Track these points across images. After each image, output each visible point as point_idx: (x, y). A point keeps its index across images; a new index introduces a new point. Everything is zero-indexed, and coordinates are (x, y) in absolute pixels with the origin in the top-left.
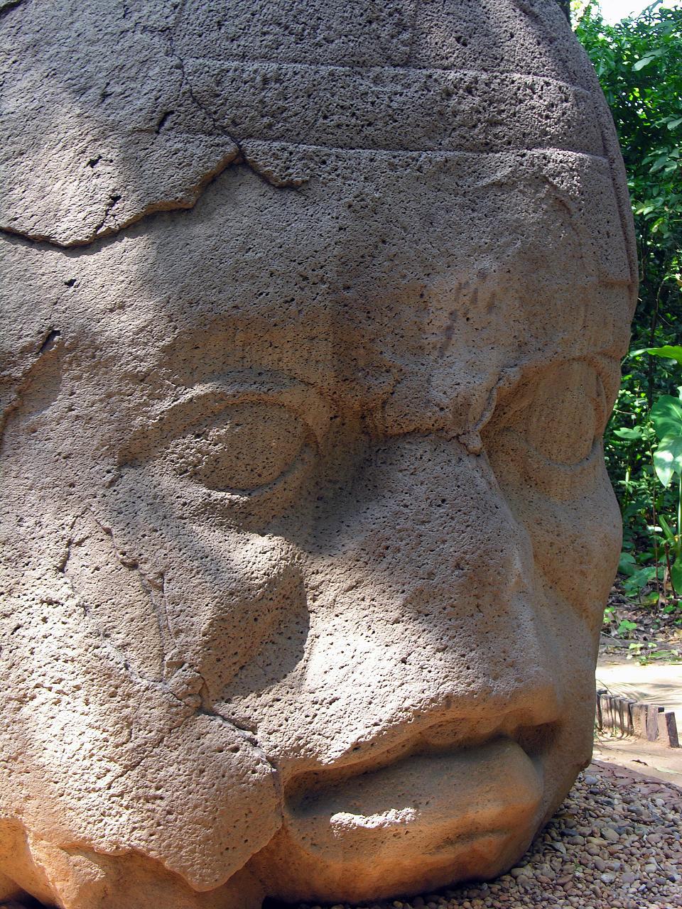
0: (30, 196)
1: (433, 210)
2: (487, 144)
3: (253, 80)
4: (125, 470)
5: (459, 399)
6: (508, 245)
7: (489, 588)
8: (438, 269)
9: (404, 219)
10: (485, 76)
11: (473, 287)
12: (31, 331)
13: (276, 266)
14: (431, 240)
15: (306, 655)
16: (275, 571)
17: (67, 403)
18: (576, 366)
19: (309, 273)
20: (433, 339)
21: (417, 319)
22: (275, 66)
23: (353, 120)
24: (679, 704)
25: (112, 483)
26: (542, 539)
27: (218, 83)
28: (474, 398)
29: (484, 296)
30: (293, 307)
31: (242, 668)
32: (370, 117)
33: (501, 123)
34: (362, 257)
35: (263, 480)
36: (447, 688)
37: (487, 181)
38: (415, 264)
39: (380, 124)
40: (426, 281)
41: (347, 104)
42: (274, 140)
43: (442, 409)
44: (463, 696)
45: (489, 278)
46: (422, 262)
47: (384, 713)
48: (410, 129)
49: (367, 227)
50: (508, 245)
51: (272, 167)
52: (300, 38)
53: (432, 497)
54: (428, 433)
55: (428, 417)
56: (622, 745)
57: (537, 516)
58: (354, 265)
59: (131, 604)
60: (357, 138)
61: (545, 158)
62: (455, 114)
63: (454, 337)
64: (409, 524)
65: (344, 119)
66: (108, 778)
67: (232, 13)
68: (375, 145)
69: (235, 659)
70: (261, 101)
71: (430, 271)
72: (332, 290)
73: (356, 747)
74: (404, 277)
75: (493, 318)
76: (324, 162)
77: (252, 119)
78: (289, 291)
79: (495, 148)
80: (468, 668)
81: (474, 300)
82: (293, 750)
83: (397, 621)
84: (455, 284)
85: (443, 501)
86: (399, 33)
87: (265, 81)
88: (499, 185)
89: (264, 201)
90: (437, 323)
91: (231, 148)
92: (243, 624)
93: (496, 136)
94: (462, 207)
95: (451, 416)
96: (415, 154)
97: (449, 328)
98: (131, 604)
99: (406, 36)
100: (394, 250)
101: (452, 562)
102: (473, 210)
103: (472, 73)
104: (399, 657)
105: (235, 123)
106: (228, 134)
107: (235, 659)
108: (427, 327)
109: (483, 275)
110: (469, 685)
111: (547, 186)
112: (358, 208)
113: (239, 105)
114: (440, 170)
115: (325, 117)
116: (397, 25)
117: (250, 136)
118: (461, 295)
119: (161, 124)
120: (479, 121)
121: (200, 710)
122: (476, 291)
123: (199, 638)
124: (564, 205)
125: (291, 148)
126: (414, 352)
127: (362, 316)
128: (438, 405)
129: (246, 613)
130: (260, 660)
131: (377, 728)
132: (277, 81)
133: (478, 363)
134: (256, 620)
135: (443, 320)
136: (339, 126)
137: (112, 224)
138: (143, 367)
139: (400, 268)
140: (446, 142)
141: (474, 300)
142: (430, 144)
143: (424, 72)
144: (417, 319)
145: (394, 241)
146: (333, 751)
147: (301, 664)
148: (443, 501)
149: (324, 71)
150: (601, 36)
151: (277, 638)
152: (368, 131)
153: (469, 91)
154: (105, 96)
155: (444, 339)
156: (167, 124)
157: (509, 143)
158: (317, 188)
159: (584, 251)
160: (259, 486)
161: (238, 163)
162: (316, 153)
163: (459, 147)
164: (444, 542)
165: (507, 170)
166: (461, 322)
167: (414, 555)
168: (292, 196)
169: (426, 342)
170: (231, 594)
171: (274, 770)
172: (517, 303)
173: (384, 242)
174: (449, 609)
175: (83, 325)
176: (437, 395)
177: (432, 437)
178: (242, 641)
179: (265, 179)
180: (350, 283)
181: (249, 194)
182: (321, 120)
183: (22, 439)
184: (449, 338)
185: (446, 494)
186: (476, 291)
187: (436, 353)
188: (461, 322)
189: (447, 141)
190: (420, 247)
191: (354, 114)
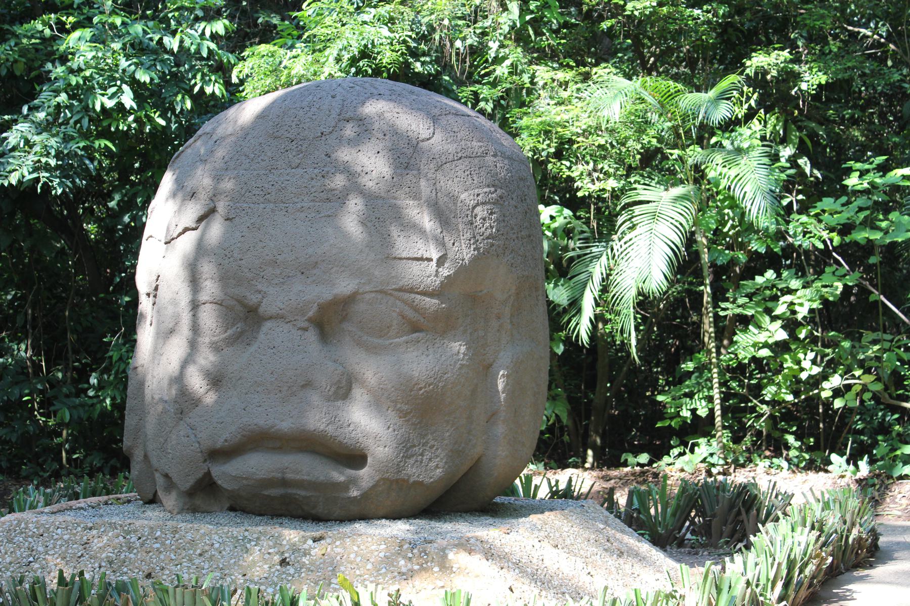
19: (227, 253)
32: (269, 191)
39: (273, 193)
65: (257, 193)
163: (313, 201)
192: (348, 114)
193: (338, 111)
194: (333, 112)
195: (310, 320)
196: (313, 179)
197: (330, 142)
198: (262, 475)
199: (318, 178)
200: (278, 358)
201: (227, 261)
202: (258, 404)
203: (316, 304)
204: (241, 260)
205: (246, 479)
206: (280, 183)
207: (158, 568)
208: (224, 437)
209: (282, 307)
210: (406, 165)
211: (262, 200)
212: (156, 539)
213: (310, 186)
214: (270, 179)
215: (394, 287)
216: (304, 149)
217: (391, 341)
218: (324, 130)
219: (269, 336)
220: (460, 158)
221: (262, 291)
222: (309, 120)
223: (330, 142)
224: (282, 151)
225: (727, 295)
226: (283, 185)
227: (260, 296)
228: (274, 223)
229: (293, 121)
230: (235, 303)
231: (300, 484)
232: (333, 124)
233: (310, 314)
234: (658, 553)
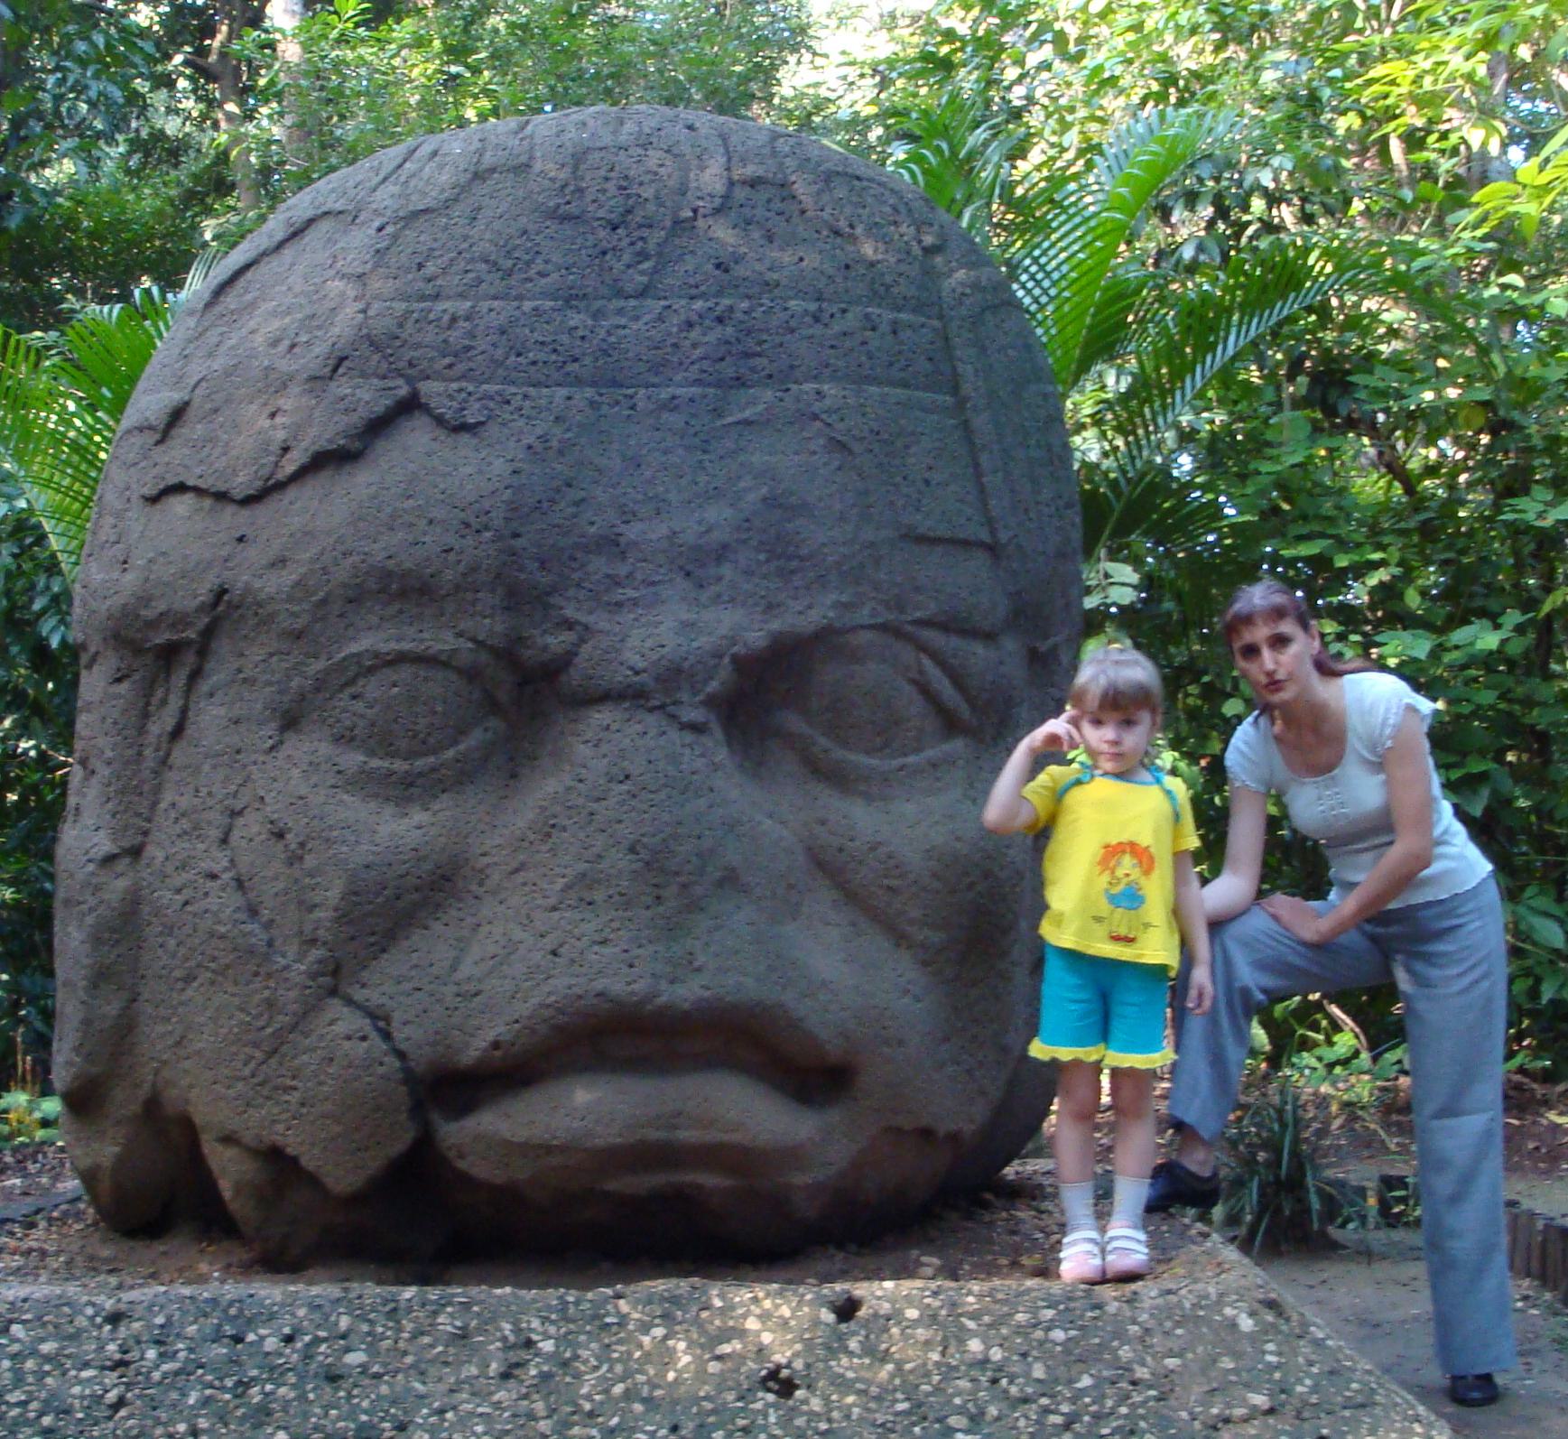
0: (216, 452)
1: (644, 452)
3: (439, 319)
4: (286, 735)
10: (745, 305)
12: (203, 592)
13: (438, 513)
17: (236, 665)
19: (472, 520)
22: (469, 304)
23: (554, 357)
25: (272, 748)
27: (401, 325)
30: (452, 557)
32: (577, 352)
33: (759, 355)
37: (730, 420)
39: (588, 360)
41: (548, 339)
42: (452, 380)
47: (523, 1009)
51: (446, 408)
52: (509, 273)
55: (621, 677)
56: (1460, 975)
59: (276, 878)
62: (694, 346)
64: (581, 801)
65: (541, 356)
66: (252, 1065)
67: (437, 253)
68: (579, 382)
70: (445, 341)
72: (499, 537)
73: (496, 1045)
74: (592, 523)
76: (508, 402)
77: (432, 359)
78: (451, 540)
83: (554, 909)
85: (627, 777)
86: (639, 262)
87: (454, 319)
88: (747, 423)
89: (435, 446)
91: (403, 391)
93: (753, 370)
96: (630, 391)
98: (276, 878)
99: (646, 265)
101: (626, 844)
102: (705, 452)
103: (727, 302)
104: (549, 947)
106: (402, 376)
110: (629, 984)
113: (418, 346)
115: (519, 355)
116: (639, 254)
117: (428, 378)
119: (335, 370)
121: (333, 992)
123: (330, 914)
125: (471, 388)
128: (631, 668)
131: (516, 1026)
132: (467, 319)
137: (281, 475)
138: (299, 623)
140: (678, 378)
142: (655, 380)
143: (663, 303)
146: (473, 1050)
149: (528, 305)
150: (1015, 286)
152: (571, 367)
153: (720, 320)
154: (293, 346)
156: (341, 371)
158: (493, 430)
161: (410, 406)
162: (498, 393)
163: (698, 382)
164: (620, 822)
165: (760, 408)
167: (582, 835)
168: (465, 438)
174: (617, 898)
175: (247, 583)
179: (440, 421)
180: (522, 530)
181: (416, 437)
182: (513, 358)
183: (202, 705)
185: (634, 770)
190: (620, 491)
191: (555, 351)
195: (710, 702)
198: (609, 1135)
199: (707, 322)
201: (470, 541)
202: (597, 938)
203: (726, 660)
204: (516, 535)
205: (563, 1149)
207: (387, 1425)
208: (491, 1035)
209: (641, 665)
211: (556, 376)
212: (343, 1337)
213: (687, 343)
214: (572, 323)
215: (918, 614)
216: (651, 247)
217: (901, 761)
219: (604, 748)
221: (578, 623)
225: (55, 642)
226: (613, 339)
227: (568, 637)
230: (484, 657)
231: (709, 1156)
233: (713, 686)
234: (356, 1287)
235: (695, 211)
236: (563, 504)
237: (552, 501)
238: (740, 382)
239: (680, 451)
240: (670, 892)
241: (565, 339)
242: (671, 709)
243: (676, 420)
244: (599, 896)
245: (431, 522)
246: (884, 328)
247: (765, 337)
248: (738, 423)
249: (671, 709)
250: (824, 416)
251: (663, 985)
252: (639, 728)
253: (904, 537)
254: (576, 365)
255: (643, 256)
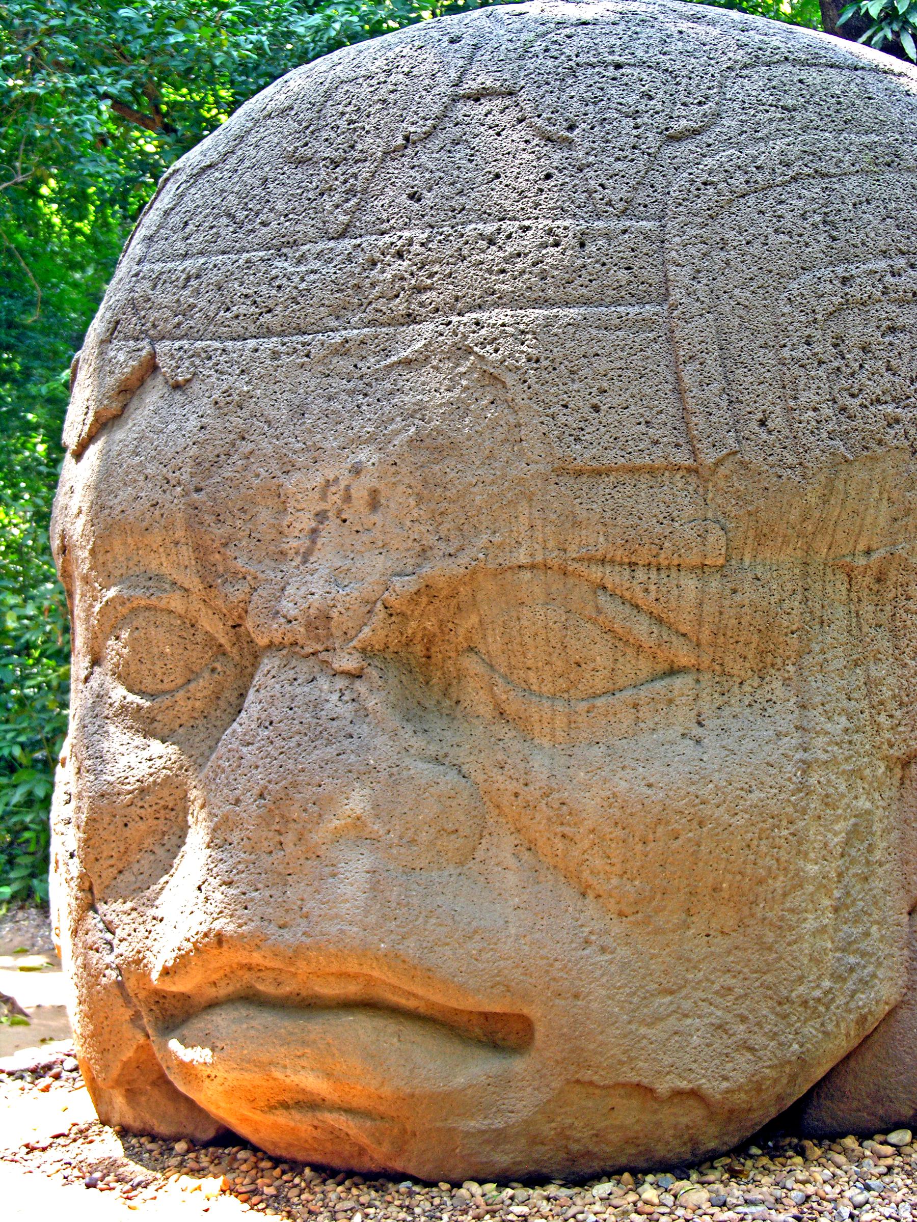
2: (409, 315)
5: (311, 611)
6: (397, 432)
7: (292, 825)
8: (298, 465)
9: (272, 413)
11: (343, 484)
14: (297, 433)
15: (173, 870)
16: (151, 779)
18: (526, 575)
20: (294, 543)
21: (276, 522)
24: (3, 968)
26: (502, 787)
28: (335, 610)
29: (360, 493)
31: (120, 872)
32: (270, 303)
33: (430, 288)
34: (218, 456)
35: (166, 686)
36: (221, 924)
37: (394, 359)
38: (272, 461)
40: (283, 479)
43: (290, 622)
44: (231, 937)
45: (364, 472)
46: (281, 458)
48: (311, 310)
49: (227, 424)
50: (397, 432)
53: (263, 717)
54: (281, 647)
57: (500, 758)
58: (207, 465)
60: (252, 328)
61: (477, 324)
62: (373, 285)
63: (320, 542)
65: (243, 309)
69: (112, 862)
71: (290, 468)
72: (186, 494)
75: (377, 518)
79: (418, 318)
80: (246, 908)
81: (348, 498)
82: (134, 962)
84: (319, 480)
88: (407, 363)
90: (299, 526)
92: (112, 827)
93: (422, 305)
94: (351, 393)
95: (302, 630)
97: (314, 531)
100: (251, 446)
105: (154, 326)
107: (112, 862)
108: (286, 530)
109: (356, 470)
110: (240, 926)
111: (472, 358)
112: (222, 404)
114: (336, 352)
118: (329, 493)
120: (403, 289)
122: (348, 488)
124: (496, 378)
126: (276, 557)
127: (209, 519)
128: (285, 617)
129: (115, 816)
130: (136, 867)
133: (354, 570)
134: (126, 825)
135: (306, 522)
136: (237, 317)
139: (255, 466)
141: (348, 498)
144: (276, 522)
145: (252, 438)
147: (166, 878)
148: (271, 723)
151: (157, 849)
153: (400, 255)
155: (308, 543)
157: (437, 310)
159: (523, 432)
160: (164, 692)
163: (371, 323)
166: (332, 524)
169: (287, 546)
170: (103, 796)
171: (120, 978)
172: (412, 502)
173: (244, 439)
176: (287, 607)
177: (284, 652)
178: (114, 845)
180: (203, 484)
184: (314, 542)
186: (348, 488)
187: (299, 559)
188: (332, 524)
189: (356, 319)
192: (480, 80)
193: (454, 75)
194: (441, 79)
196: (374, 264)
197: (424, 159)
200: (275, 754)
206: (296, 279)
210: (621, 206)
218: (412, 129)
220: (794, 179)
222: (379, 106)
223: (424, 159)
224: (311, 195)
226: (303, 286)
228: (276, 387)
229: (343, 114)
232: (437, 109)
235: (407, 138)
236: (236, 457)
237: (228, 455)
238: (411, 318)
239: (343, 396)
240: (289, 838)
241: (264, 289)
242: (324, 656)
243: (343, 364)
244: (235, 837)
245: (146, 478)
246: (568, 241)
247: (436, 268)
248: (400, 362)
249: (324, 656)
250: (476, 349)
251: (272, 929)
252: (291, 674)
253: (560, 471)
254: (269, 315)
255: (351, 192)
